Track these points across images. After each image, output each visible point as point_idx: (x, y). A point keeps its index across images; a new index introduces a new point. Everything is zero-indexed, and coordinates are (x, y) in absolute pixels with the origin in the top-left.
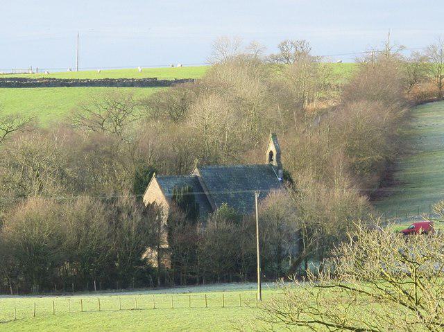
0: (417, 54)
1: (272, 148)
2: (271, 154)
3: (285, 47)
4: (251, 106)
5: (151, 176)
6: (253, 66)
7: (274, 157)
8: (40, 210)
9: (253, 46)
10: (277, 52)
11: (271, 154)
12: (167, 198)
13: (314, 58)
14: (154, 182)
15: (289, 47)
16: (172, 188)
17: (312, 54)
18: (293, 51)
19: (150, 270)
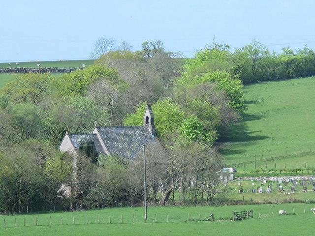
0: (239, 51)
1: (148, 114)
2: (147, 118)
3: (147, 46)
4: (195, 59)
5: (64, 134)
6: (124, 58)
7: (149, 121)
8: (4, 68)
9: (124, 44)
10: (141, 49)
11: (147, 118)
12: (76, 148)
13: (167, 54)
14: (67, 137)
15: (149, 46)
16: (79, 142)
17: (166, 50)
18: (152, 48)
19: (65, 200)
